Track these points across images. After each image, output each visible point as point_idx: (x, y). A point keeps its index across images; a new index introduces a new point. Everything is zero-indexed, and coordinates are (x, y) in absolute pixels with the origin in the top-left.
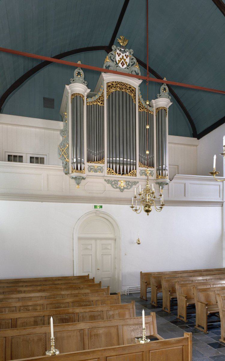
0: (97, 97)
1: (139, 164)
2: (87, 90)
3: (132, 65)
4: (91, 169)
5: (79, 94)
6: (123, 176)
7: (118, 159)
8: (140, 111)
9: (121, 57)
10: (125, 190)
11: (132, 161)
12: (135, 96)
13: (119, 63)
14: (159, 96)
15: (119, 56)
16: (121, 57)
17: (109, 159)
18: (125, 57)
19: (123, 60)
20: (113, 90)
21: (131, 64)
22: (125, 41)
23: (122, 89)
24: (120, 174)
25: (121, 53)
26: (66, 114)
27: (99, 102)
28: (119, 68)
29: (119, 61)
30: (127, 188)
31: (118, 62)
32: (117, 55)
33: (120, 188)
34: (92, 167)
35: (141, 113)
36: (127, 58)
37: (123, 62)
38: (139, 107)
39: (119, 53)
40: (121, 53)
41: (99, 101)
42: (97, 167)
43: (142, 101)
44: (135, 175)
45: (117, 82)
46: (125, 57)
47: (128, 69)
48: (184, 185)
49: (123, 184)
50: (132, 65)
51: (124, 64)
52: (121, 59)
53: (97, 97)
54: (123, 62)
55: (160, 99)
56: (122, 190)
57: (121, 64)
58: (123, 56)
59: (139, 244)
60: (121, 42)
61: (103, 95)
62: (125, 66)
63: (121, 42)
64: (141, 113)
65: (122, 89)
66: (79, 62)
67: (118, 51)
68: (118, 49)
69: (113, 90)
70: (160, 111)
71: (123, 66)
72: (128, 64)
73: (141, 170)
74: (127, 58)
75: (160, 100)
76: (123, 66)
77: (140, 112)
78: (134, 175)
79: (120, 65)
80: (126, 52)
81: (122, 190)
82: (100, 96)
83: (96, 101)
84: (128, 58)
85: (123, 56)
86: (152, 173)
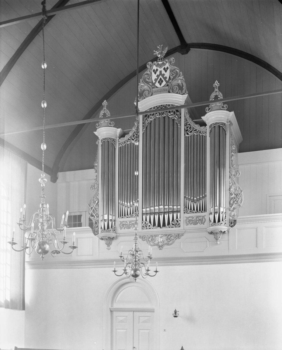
0: (131, 134)
1: (184, 210)
2: (117, 130)
3: (174, 78)
4: (189, 221)
5: (105, 139)
6: (164, 229)
7: (175, 207)
8: (187, 136)
9: (158, 73)
10: (166, 247)
11: (175, 207)
12: (180, 118)
13: (155, 83)
14: (208, 110)
15: (155, 73)
16: (158, 73)
17: (172, 207)
18: (163, 72)
19: (161, 77)
20: (151, 119)
21: (172, 77)
22: (164, 51)
23: (163, 115)
24: (159, 225)
25: (158, 68)
26: (96, 164)
27: (133, 140)
28: (156, 89)
29: (156, 80)
30: (168, 244)
31: (154, 82)
32: (153, 73)
33: (157, 245)
34: (191, 219)
35: (190, 138)
36: (166, 71)
37: (161, 79)
38: (186, 131)
39: (155, 69)
40: (158, 68)
41: (133, 138)
42: (130, 222)
43: (190, 121)
44: (179, 226)
45: (156, 106)
46: (163, 72)
47: (167, 85)
48: (255, 229)
49: (160, 240)
50: (174, 78)
51: (162, 81)
52: (158, 76)
53: (131, 134)
54: (161, 79)
55: (211, 113)
56: (160, 247)
57: (159, 82)
58: (161, 72)
59: (176, 317)
60: (159, 54)
61: (138, 130)
62: (164, 83)
63: (159, 54)
64: (190, 138)
65: (163, 115)
66: (104, 101)
67: (155, 68)
68: (155, 64)
69: (151, 119)
70: (219, 129)
71: (160, 85)
72: (167, 79)
73: (187, 218)
74: (166, 71)
75: (210, 114)
76: (160, 85)
77: (188, 137)
78: (177, 226)
79: (157, 84)
80: (165, 64)
81: (160, 247)
82: (135, 132)
83: (129, 140)
84: (168, 71)
85: (161, 72)
86: (204, 219)
